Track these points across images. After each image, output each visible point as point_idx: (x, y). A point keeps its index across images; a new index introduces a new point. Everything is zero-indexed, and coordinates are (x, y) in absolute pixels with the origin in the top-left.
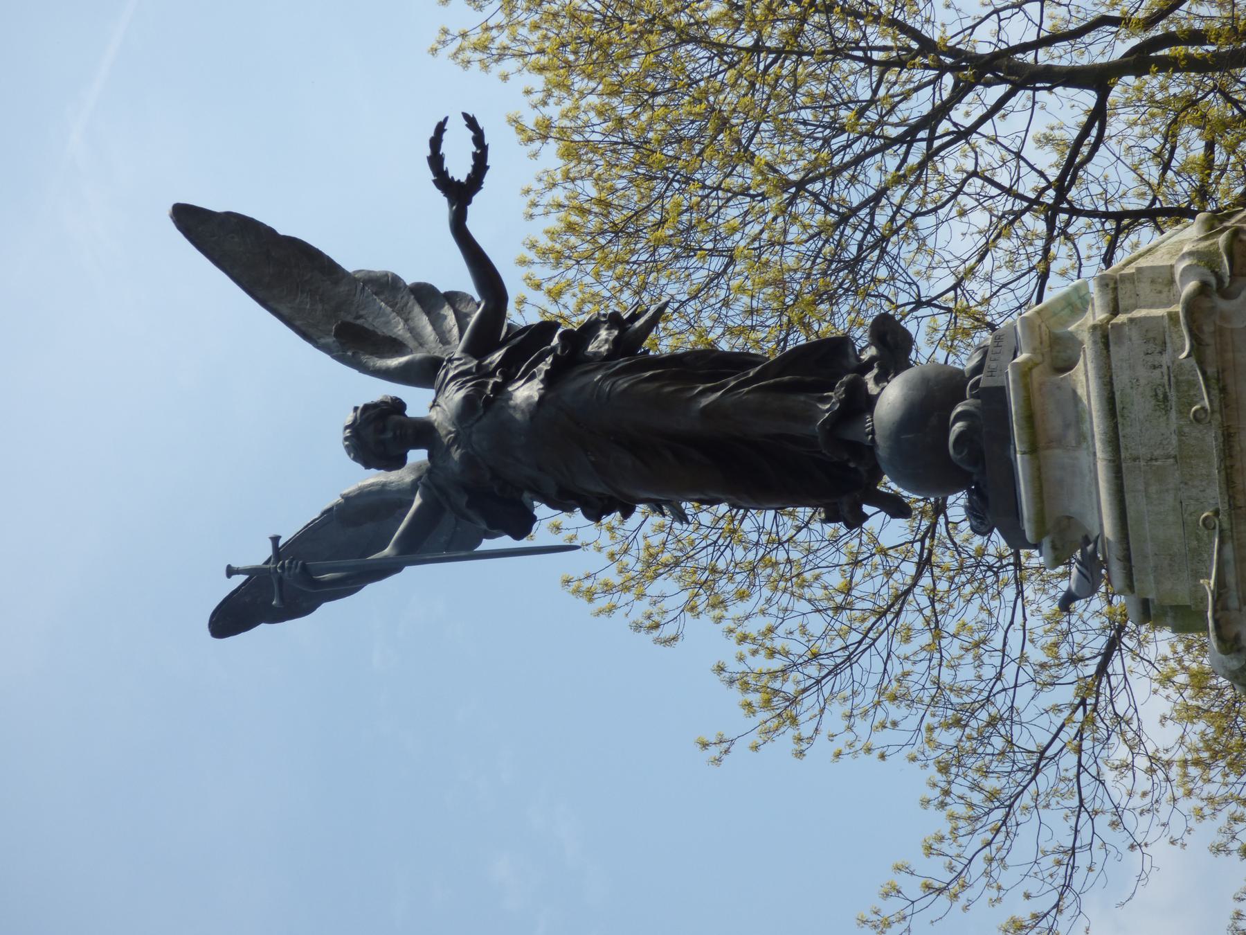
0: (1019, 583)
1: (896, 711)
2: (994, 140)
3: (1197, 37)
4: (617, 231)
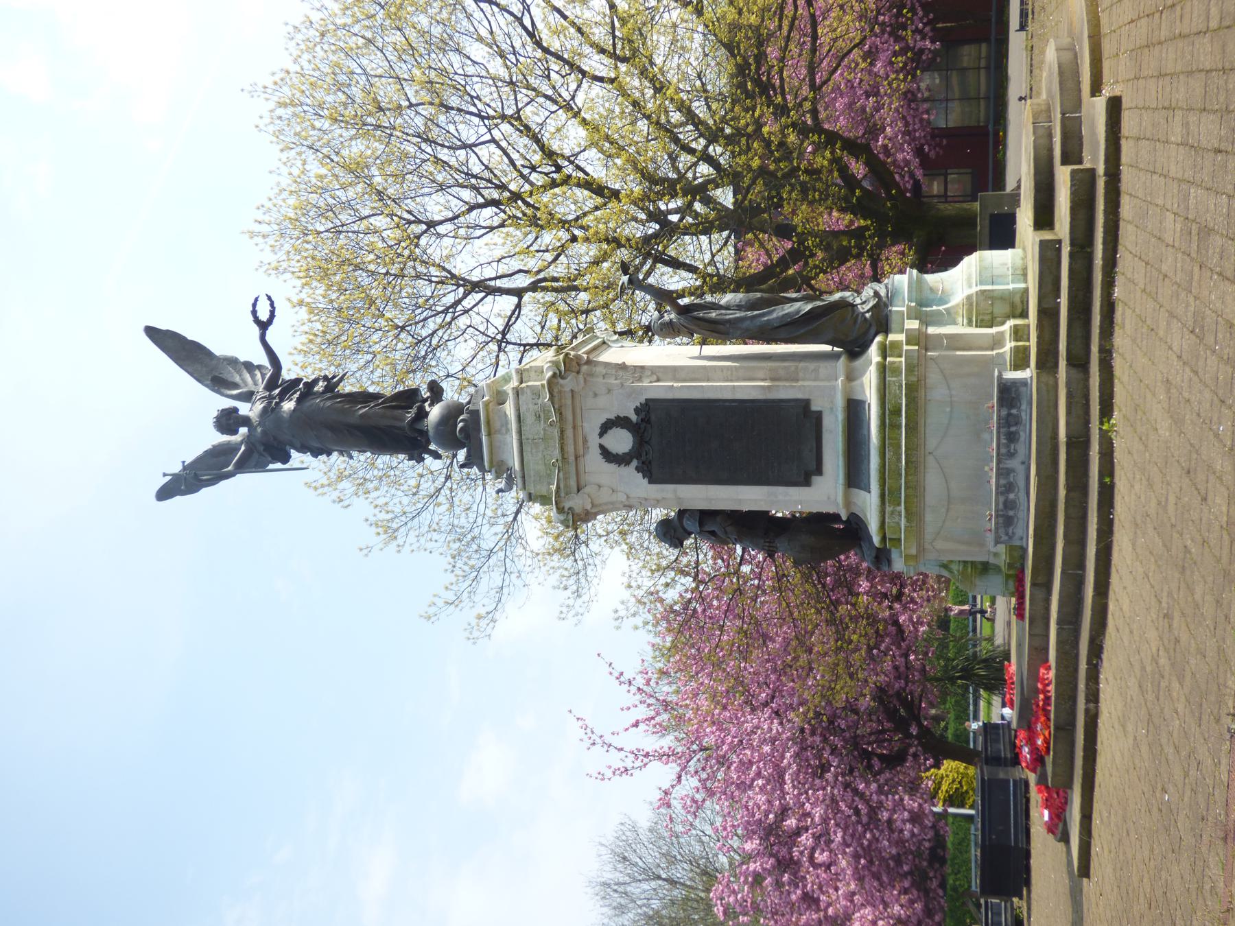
0: (484, 485)
1: (435, 536)
2: (478, 314)
3: (555, 279)
4: (330, 343)
